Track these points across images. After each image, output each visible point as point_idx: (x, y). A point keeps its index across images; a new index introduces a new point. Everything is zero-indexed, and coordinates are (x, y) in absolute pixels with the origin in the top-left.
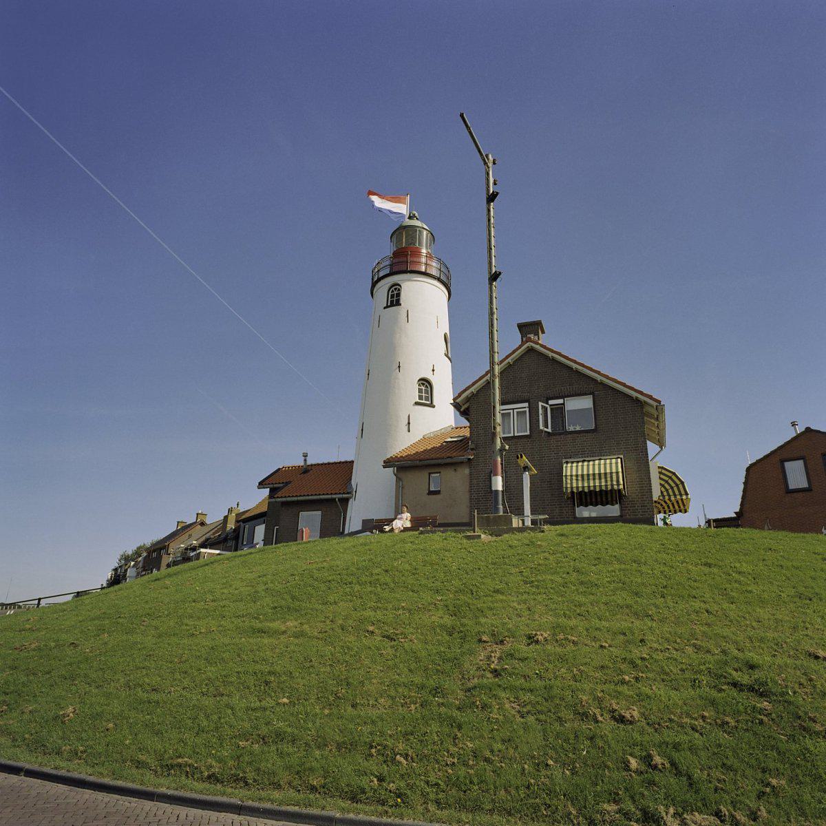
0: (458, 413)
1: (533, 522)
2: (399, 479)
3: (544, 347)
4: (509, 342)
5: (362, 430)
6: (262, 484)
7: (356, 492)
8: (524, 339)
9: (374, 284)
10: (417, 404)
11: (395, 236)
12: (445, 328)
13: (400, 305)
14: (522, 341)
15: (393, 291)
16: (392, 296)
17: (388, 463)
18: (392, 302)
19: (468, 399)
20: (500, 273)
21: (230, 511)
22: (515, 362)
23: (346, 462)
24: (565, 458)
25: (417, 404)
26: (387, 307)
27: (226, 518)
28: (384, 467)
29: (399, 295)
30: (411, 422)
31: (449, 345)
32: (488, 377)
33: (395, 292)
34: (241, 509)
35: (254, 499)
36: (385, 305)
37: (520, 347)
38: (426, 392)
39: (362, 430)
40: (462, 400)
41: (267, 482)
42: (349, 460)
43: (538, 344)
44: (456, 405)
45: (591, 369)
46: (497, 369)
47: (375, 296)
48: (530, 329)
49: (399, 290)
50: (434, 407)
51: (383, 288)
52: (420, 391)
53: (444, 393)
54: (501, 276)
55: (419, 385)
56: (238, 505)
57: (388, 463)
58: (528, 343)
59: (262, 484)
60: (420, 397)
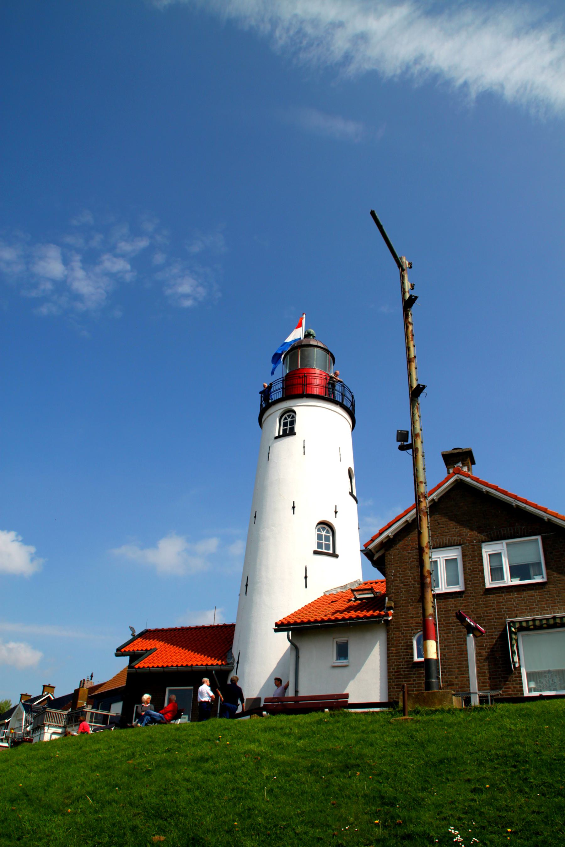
0: (369, 563)
1: (483, 700)
2: (295, 648)
3: (477, 480)
4: (436, 477)
5: (247, 585)
6: (120, 653)
7: (238, 663)
8: (451, 471)
9: (263, 412)
10: (316, 553)
11: (288, 357)
12: (349, 462)
13: (295, 434)
14: (449, 473)
15: (285, 419)
16: (285, 424)
17: (280, 627)
18: (285, 431)
19: (382, 545)
20: (424, 387)
21: (82, 683)
22: (440, 499)
23: (225, 626)
24: (510, 618)
25: (316, 553)
26: (279, 437)
27: (77, 691)
28: (276, 631)
29: (293, 423)
30: (245, 587)
31: (354, 481)
32: (409, 517)
33: (289, 420)
34: (96, 682)
35: (110, 669)
36: (277, 435)
37: (447, 479)
38: (327, 539)
39: (247, 585)
40: (375, 547)
41: (127, 649)
42: (229, 622)
43: (468, 476)
44: (368, 553)
45: (536, 507)
46: (425, 504)
47: (264, 426)
48: (457, 458)
49: (293, 417)
50: (337, 556)
51: (277, 410)
52: (319, 537)
53: (350, 542)
54: (425, 390)
55: (319, 530)
56: (92, 676)
57: (280, 627)
58: (456, 476)
59: (120, 653)
60: (320, 545)
